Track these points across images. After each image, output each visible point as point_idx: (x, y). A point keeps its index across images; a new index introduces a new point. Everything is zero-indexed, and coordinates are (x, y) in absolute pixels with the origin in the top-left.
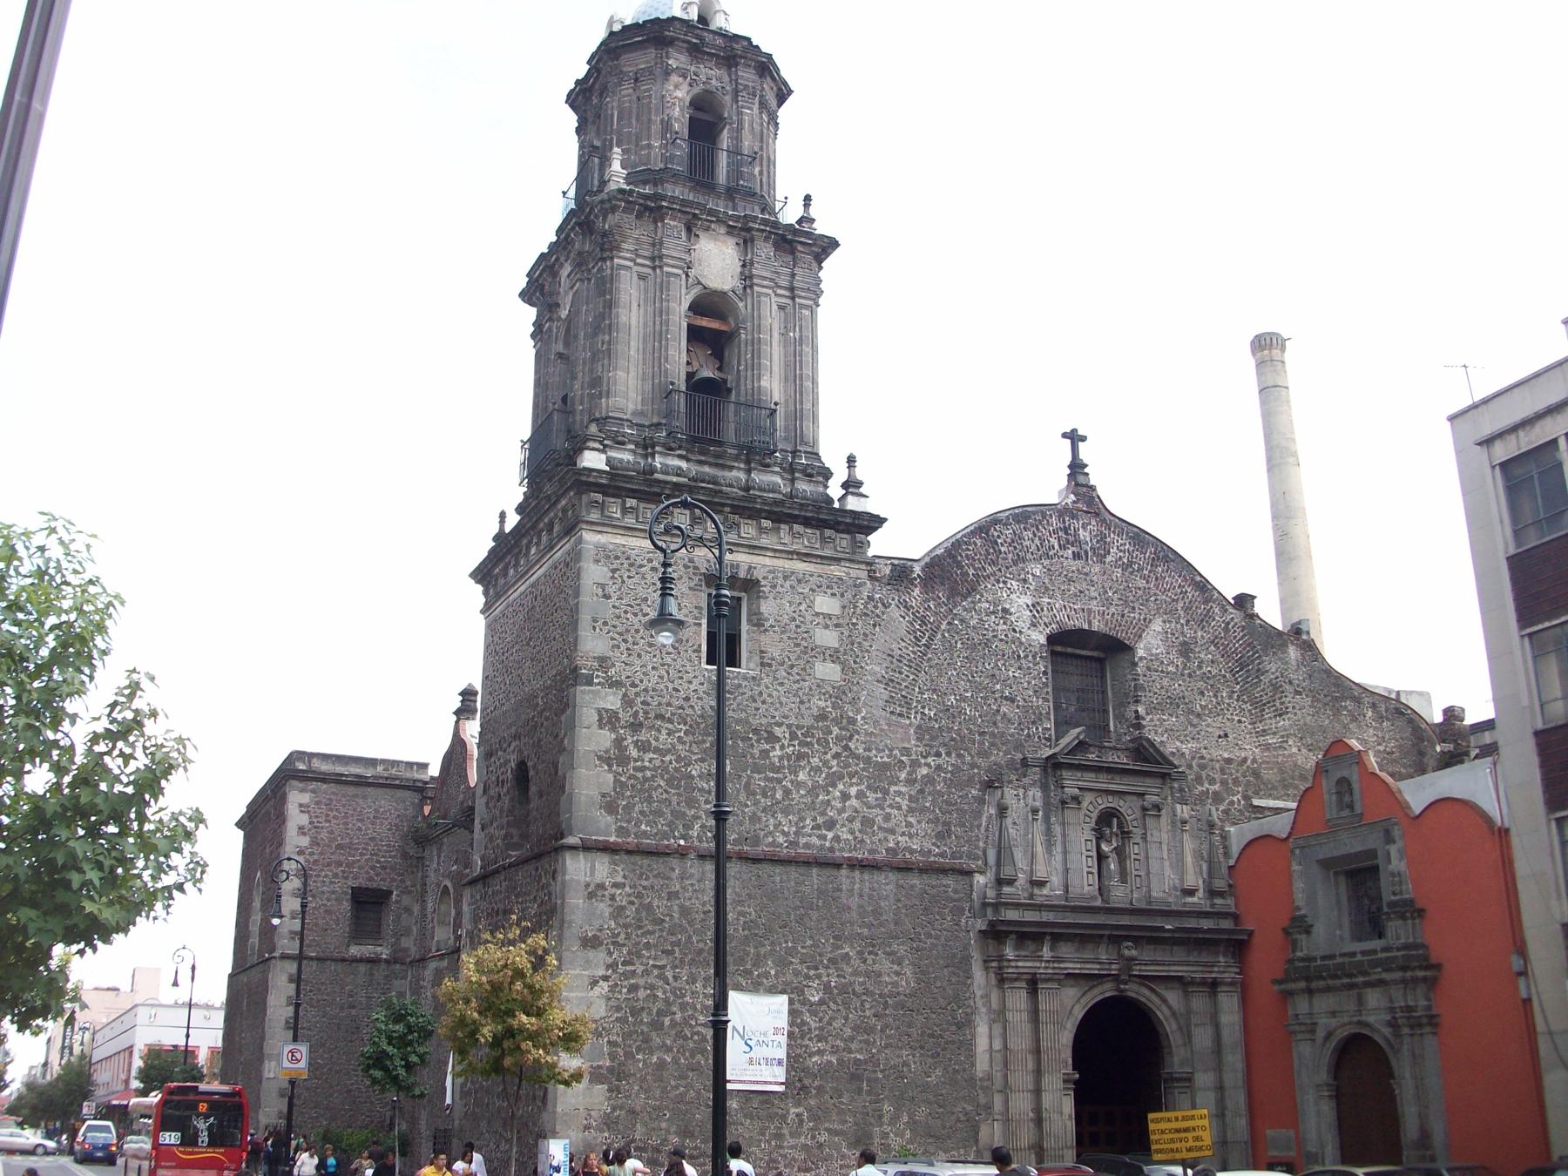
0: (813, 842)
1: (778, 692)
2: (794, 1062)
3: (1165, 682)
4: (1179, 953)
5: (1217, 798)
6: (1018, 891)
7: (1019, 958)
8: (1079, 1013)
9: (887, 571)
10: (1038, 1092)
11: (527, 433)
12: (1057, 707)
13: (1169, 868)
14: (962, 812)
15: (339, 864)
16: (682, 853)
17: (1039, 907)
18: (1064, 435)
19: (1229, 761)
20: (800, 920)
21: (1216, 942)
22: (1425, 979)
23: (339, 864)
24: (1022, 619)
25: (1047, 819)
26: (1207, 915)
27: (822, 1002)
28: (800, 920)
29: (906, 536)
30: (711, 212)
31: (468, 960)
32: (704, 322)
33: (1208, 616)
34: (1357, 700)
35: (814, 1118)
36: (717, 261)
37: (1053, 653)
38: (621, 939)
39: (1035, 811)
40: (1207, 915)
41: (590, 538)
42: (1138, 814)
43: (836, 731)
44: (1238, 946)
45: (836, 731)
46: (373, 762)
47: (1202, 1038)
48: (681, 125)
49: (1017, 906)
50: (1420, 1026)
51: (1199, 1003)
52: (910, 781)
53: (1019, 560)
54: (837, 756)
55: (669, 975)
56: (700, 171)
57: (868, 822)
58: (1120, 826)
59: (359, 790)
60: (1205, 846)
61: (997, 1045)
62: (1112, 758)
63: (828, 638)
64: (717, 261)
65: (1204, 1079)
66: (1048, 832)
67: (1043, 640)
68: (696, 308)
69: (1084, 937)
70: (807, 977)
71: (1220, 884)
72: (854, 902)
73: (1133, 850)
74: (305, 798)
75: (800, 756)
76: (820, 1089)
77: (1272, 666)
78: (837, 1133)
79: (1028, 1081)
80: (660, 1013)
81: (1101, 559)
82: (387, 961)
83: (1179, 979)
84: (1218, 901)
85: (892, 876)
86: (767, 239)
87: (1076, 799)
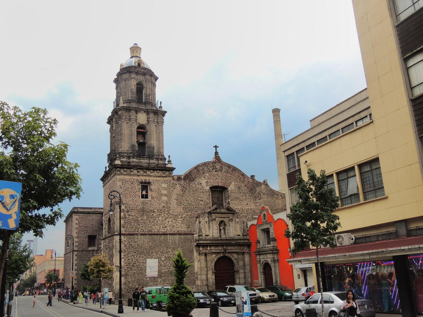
0: (162, 231)
1: (155, 203)
2: (159, 271)
3: (235, 195)
4: (236, 247)
5: (246, 217)
6: (204, 237)
7: (203, 250)
8: (216, 259)
9: (176, 178)
10: (207, 275)
11: (109, 152)
12: (212, 201)
13: (234, 231)
14: (192, 223)
15: (85, 230)
16: (137, 235)
17: (207, 240)
18: (214, 147)
19: (248, 209)
20: (160, 245)
21: (244, 245)
22: (276, 253)
23: (85, 230)
24: (204, 184)
25: (209, 223)
26: (242, 240)
27: (164, 260)
28: (160, 245)
29: (180, 171)
30: (140, 109)
31: (92, 259)
32: (141, 130)
33: (244, 180)
34: (277, 195)
35: (164, 281)
36: (142, 118)
37: (212, 191)
38: (126, 251)
39: (206, 222)
40: (242, 240)
41: (118, 177)
42: (228, 221)
43: (166, 209)
44: (249, 245)
45: (166, 209)
46: (91, 208)
47: (241, 263)
48: (135, 90)
49: (202, 240)
50: (276, 261)
51: (240, 257)
52: (181, 218)
53: (204, 173)
54: (167, 214)
55: (135, 256)
56: (139, 100)
57: (173, 226)
58: (224, 223)
59: (88, 215)
60: (242, 226)
61: (199, 266)
62: (222, 211)
63: (165, 192)
64: (142, 118)
65: (241, 271)
66: (209, 226)
67: (209, 188)
68: (138, 128)
69: (216, 245)
70: (162, 255)
71: (245, 234)
72: (170, 241)
73: (226, 228)
74: (77, 217)
75: (160, 215)
76: (165, 276)
77: (258, 189)
78: (168, 284)
79: (205, 273)
80: (134, 264)
81: (221, 171)
82: (96, 250)
83: (236, 252)
84: (245, 237)
85: (178, 236)
86: (152, 113)
87: (214, 219)
